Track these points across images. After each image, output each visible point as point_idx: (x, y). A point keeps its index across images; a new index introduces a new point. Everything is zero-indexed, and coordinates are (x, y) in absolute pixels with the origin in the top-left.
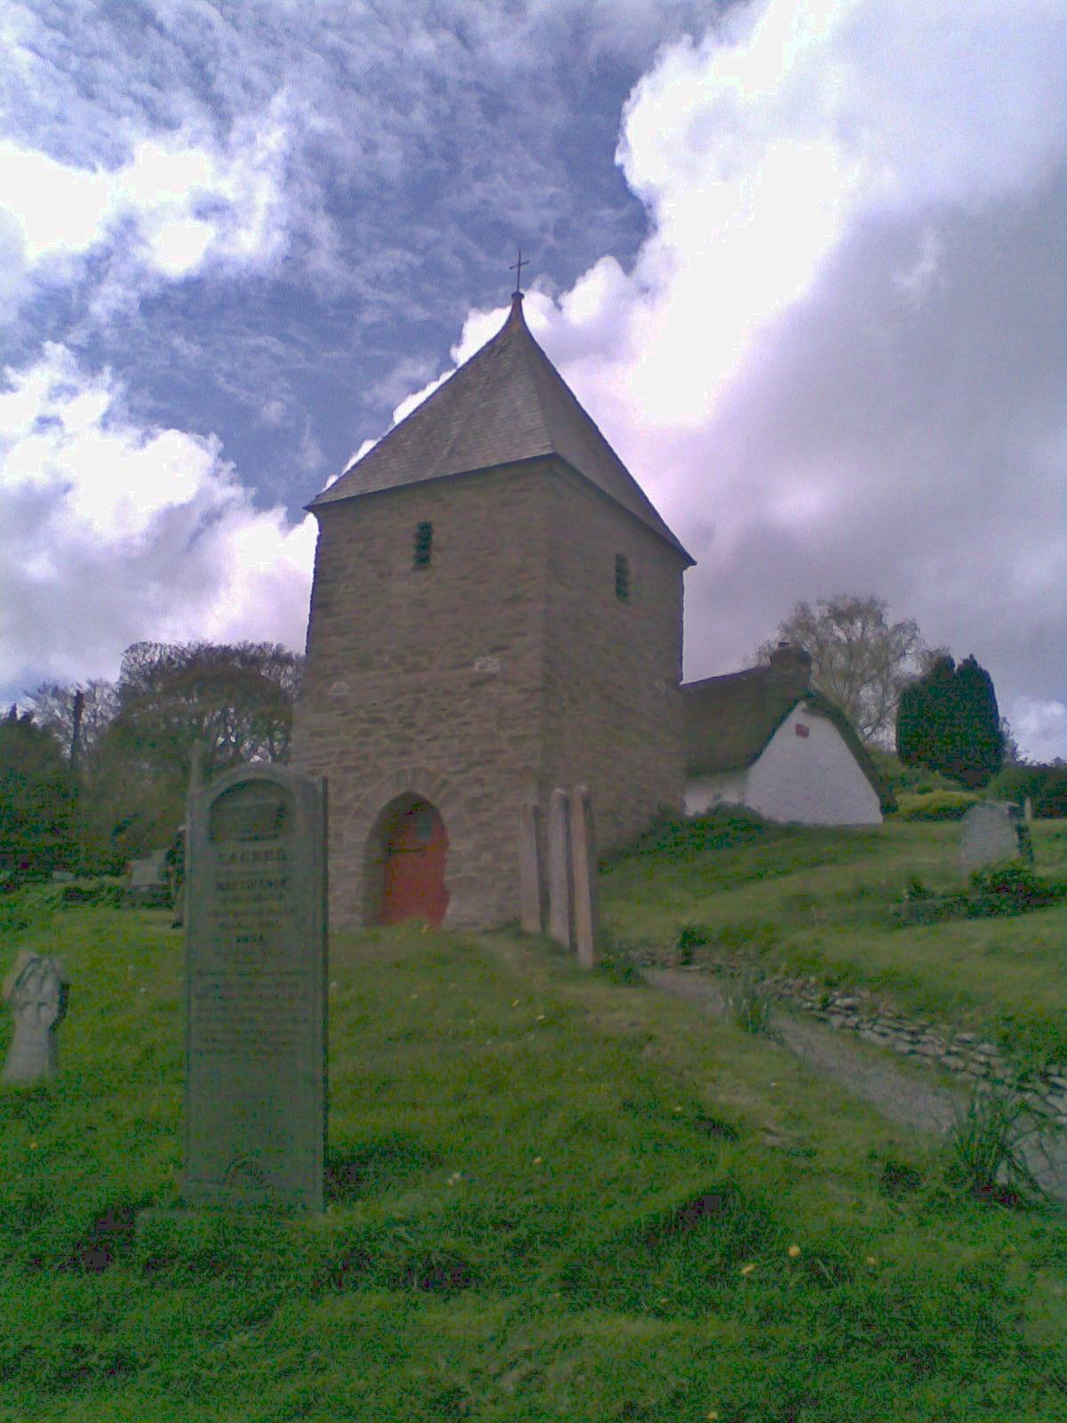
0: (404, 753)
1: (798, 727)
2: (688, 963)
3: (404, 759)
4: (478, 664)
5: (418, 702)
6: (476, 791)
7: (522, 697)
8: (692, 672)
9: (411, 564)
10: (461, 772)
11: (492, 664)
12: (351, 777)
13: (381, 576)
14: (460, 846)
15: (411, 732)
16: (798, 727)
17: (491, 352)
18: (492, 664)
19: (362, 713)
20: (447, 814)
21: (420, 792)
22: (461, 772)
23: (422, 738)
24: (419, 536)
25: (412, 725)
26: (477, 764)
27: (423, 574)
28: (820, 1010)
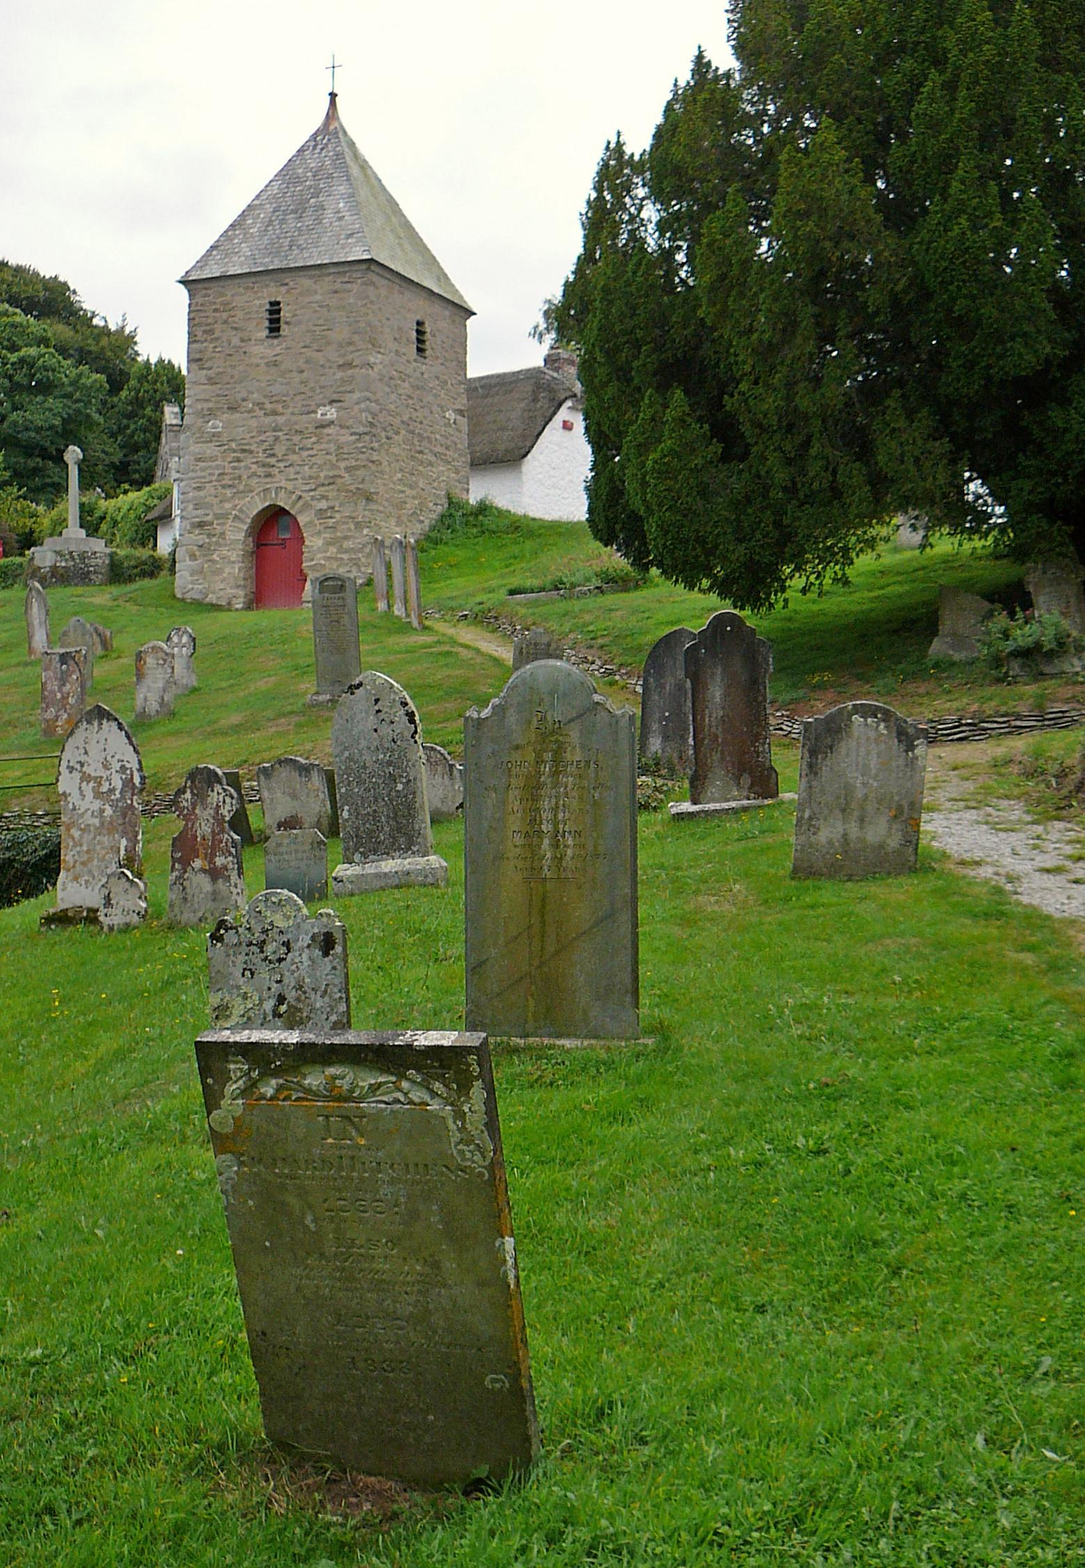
0: (269, 475)
1: (565, 422)
2: (478, 1285)
3: (268, 480)
4: (320, 412)
5: (277, 438)
6: (323, 505)
7: (354, 438)
8: (475, 370)
9: (266, 332)
10: (311, 490)
11: (331, 413)
12: (229, 492)
13: (242, 340)
14: (313, 542)
15: (272, 461)
16: (565, 422)
17: (315, 147)
18: (331, 413)
19: (233, 445)
20: (302, 520)
21: (282, 504)
22: (311, 490)
23: (282, 465)
24: (271, 312)
25: (273, 455)
26: (323, 485)
27: (276, 342)
28: (248, 607)
